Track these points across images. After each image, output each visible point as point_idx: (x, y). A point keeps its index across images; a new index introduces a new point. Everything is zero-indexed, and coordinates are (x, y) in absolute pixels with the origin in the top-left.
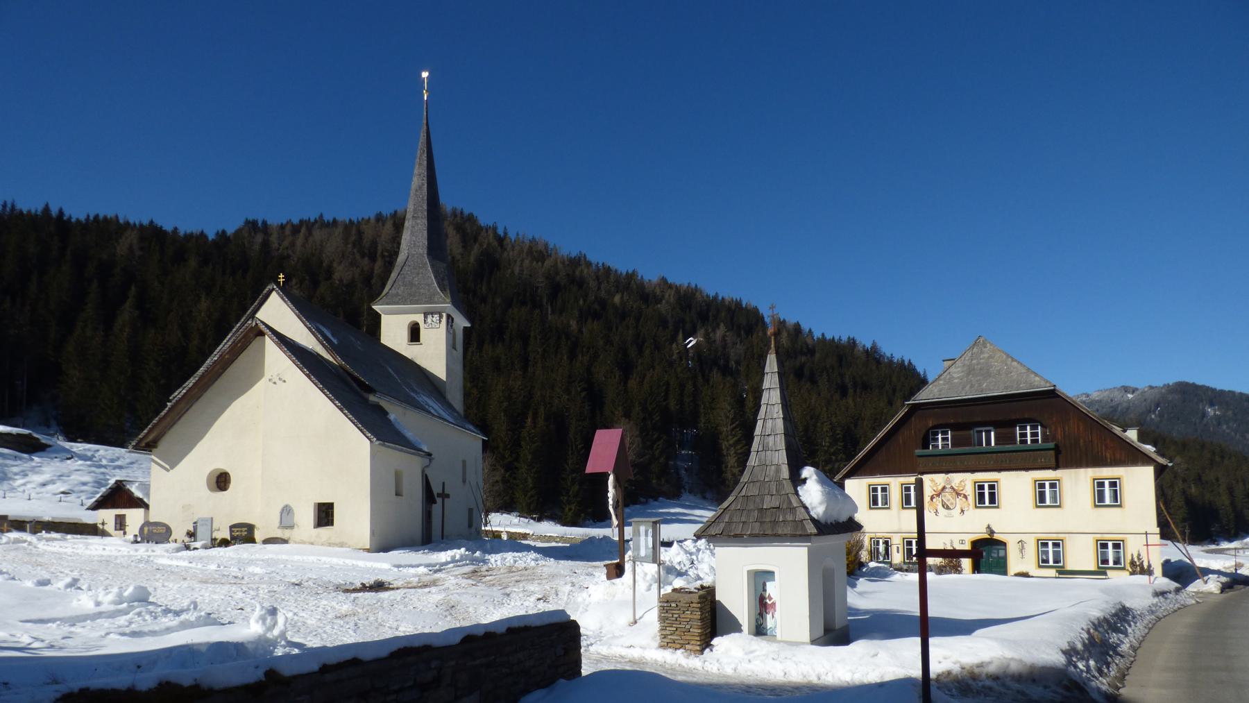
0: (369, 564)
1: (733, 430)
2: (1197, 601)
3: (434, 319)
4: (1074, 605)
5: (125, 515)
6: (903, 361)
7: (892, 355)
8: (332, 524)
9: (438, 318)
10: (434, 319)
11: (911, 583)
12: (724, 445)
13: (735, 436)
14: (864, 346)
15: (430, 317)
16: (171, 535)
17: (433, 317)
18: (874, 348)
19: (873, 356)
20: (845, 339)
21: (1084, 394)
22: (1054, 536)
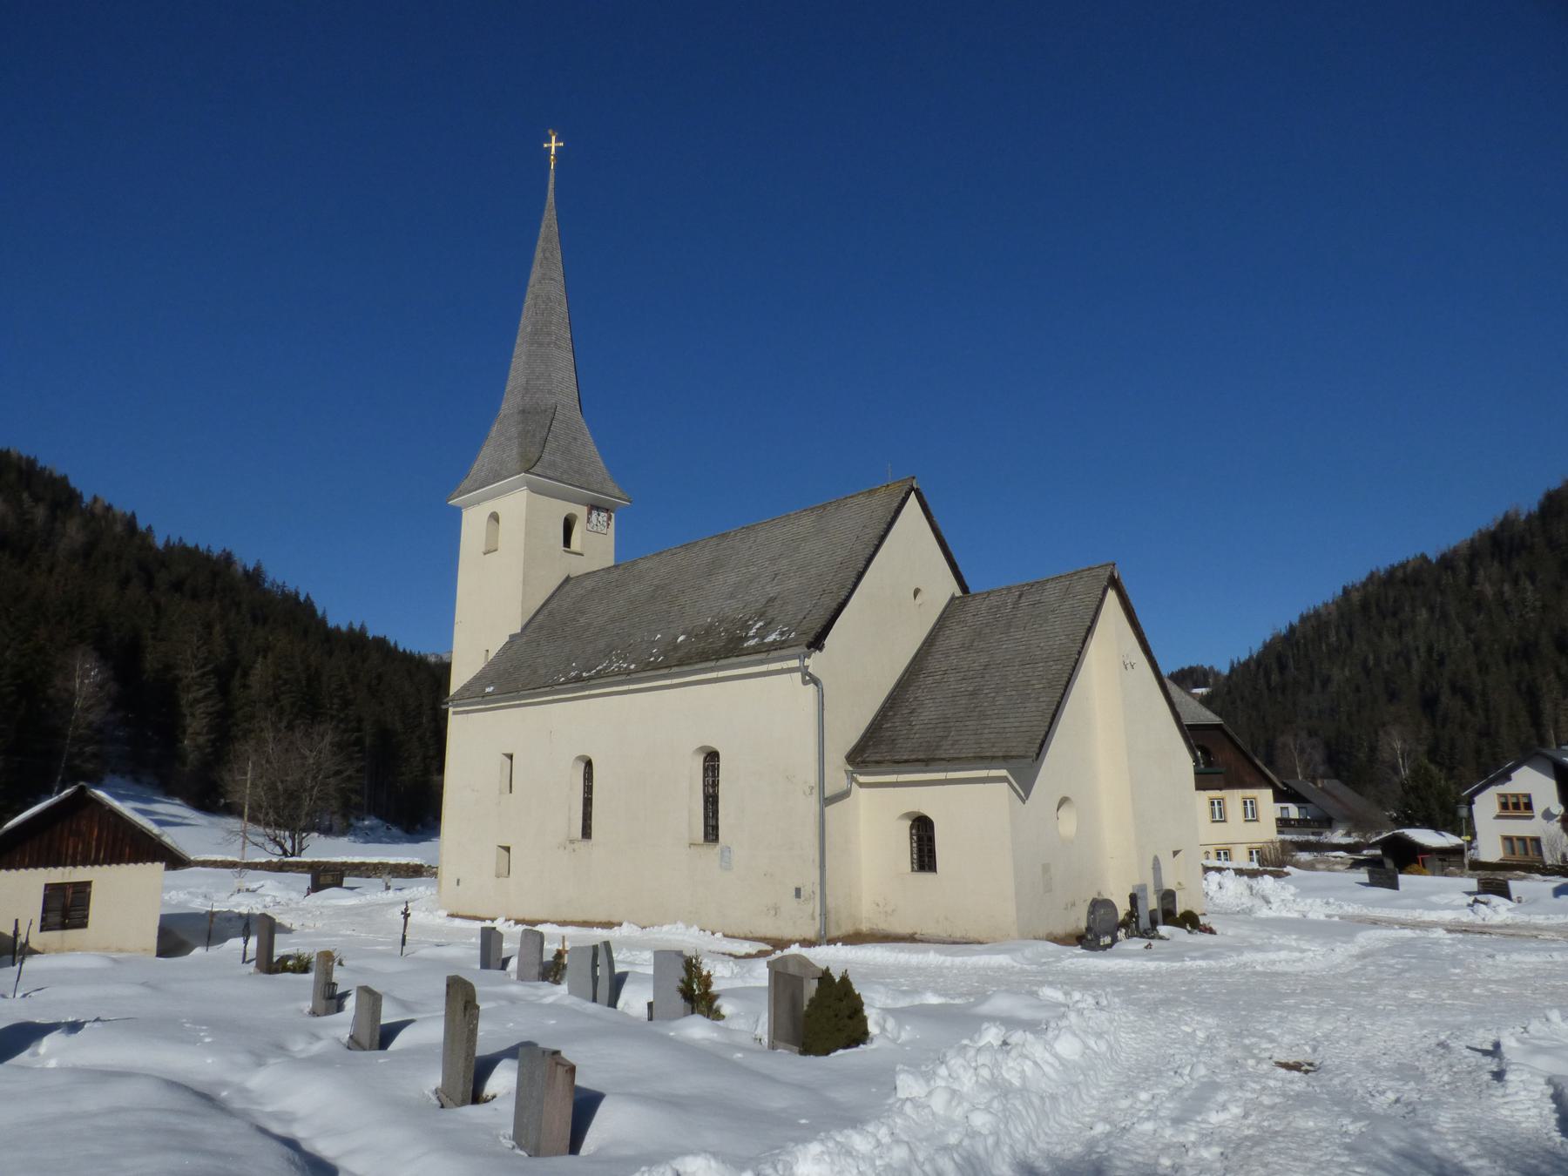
0: (958, 960)
1: (203, 675)
2: (115, 960)
3: (600, 519)
4: (966, 943)
5: (88, 884)
6: (297, 594)
7: (284, 583)
8: (47, 886)
9: (605, 519)
10: (600, 519)
11: (549, 943)
12: (185, 698)
13: (206, 686)
14: (245, 567)
15: (595, 513)
16: (1116, 910)
17: (599, 515)
18: (257, 570)
19: (254, 578)
20: (216, 551)
21: (433, 654)
22: (1224, 847)
